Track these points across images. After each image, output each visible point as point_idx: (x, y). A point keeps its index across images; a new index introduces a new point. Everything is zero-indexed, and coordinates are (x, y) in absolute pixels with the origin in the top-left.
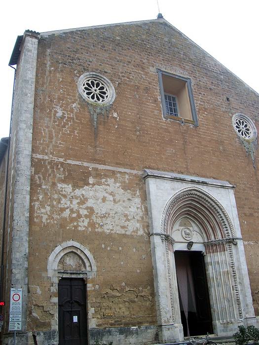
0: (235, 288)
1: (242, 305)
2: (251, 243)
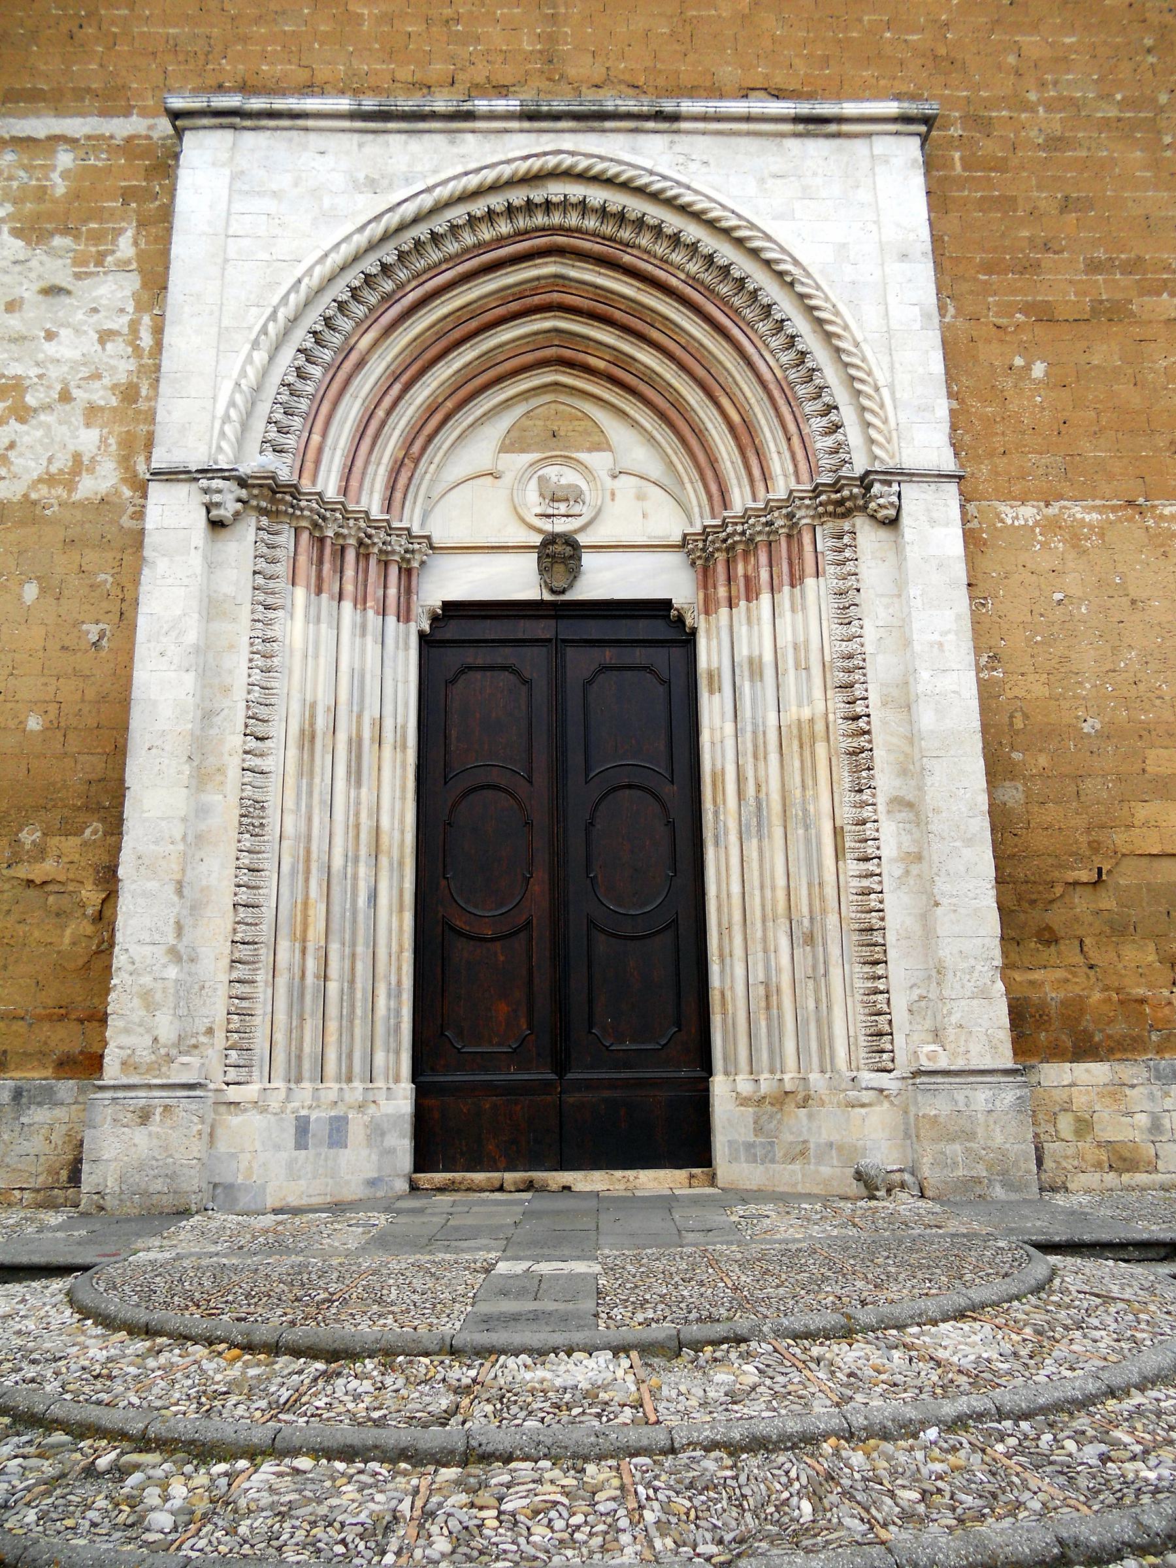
0: (855, 842)
1: (900, 971)
2: (1080, 513)
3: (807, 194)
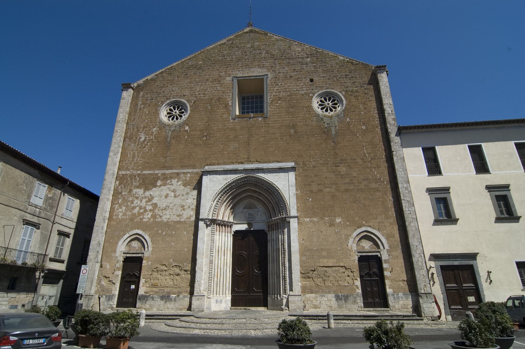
2: (315, 219)
3: (280, 178)
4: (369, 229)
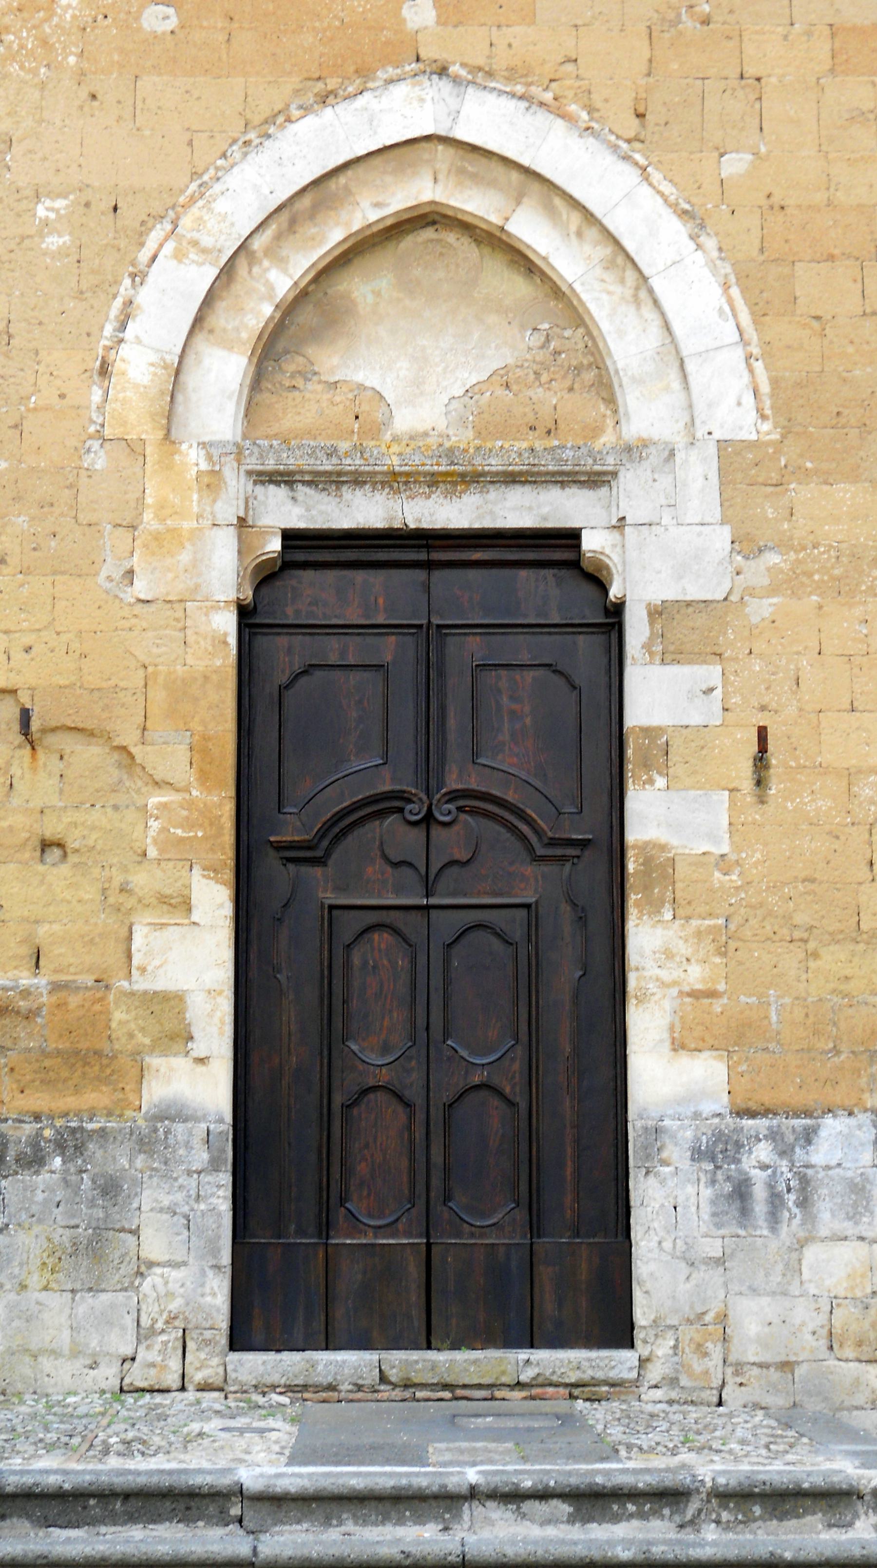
4: (489, 119)
